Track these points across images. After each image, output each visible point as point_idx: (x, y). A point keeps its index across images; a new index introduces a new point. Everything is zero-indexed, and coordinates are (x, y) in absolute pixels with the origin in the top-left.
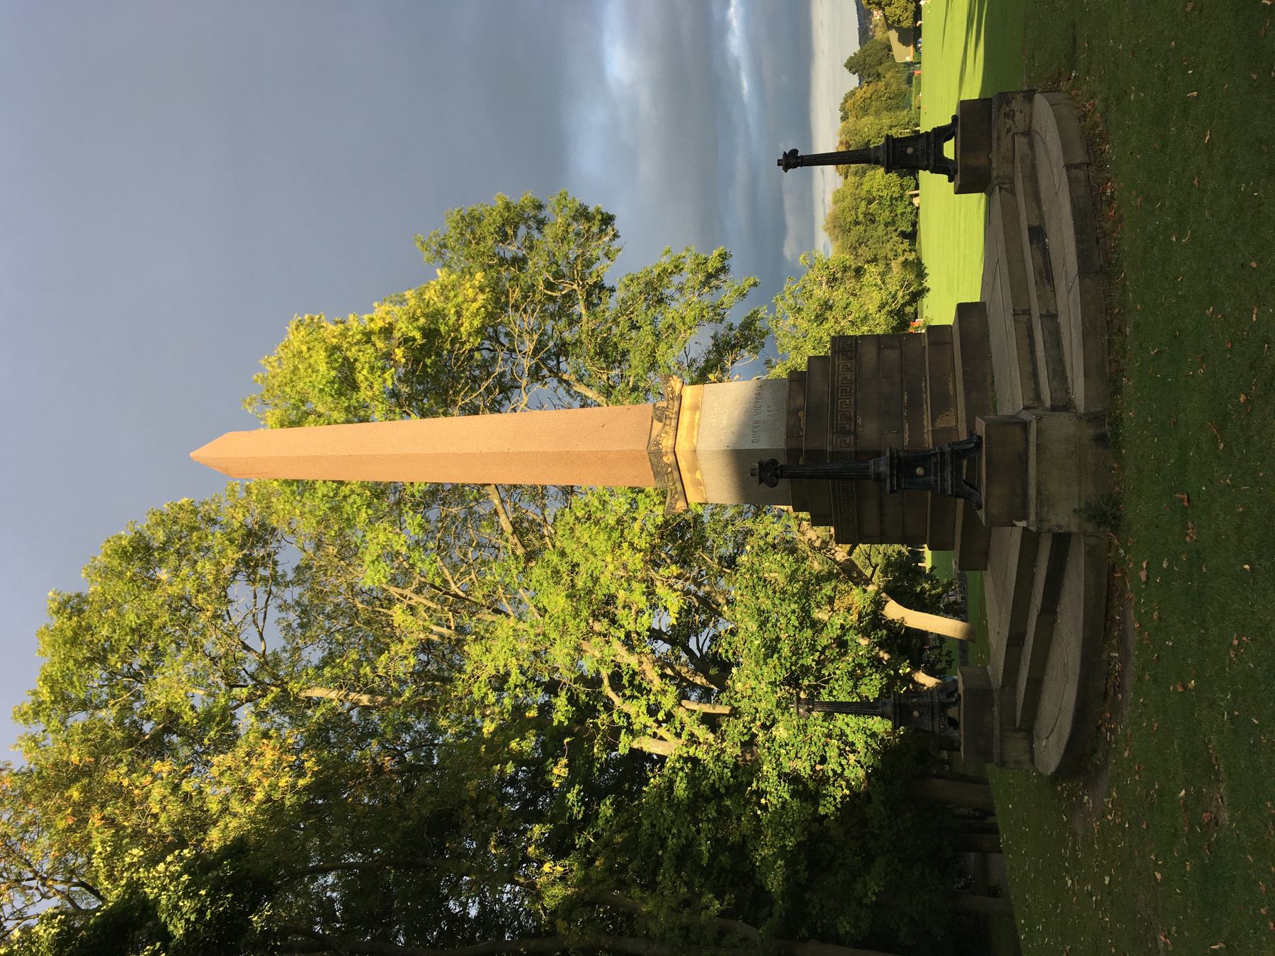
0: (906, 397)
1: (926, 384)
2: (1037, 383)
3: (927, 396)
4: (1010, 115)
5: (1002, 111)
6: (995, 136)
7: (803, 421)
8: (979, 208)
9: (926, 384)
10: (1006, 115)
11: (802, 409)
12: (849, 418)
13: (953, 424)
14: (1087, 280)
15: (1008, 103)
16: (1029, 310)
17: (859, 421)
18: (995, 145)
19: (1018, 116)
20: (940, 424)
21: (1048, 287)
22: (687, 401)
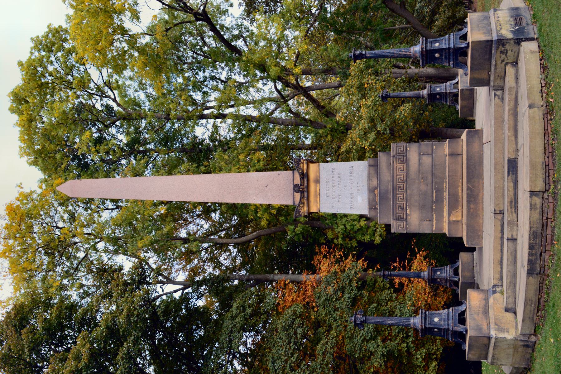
0: (434, 194)
1: (446, 185)
2: (502, 268)
3: (446, 195)
4: (505, 52)
5: (500, 50)
6: (493, 62)
7: (378, 197)
8: (469, 297)
9: (446, 185)
10: (501, 52)
11: (376, 188)
12: (402, 209)
13: (459, 219)
14: (531, 278)
15: (503, 45)
16: (503, 211)
17: (408, 212)
18: (493, 68)
19: (510, 53)
20: (453, 218)
21: (514, 215)
22: (312, 176)
